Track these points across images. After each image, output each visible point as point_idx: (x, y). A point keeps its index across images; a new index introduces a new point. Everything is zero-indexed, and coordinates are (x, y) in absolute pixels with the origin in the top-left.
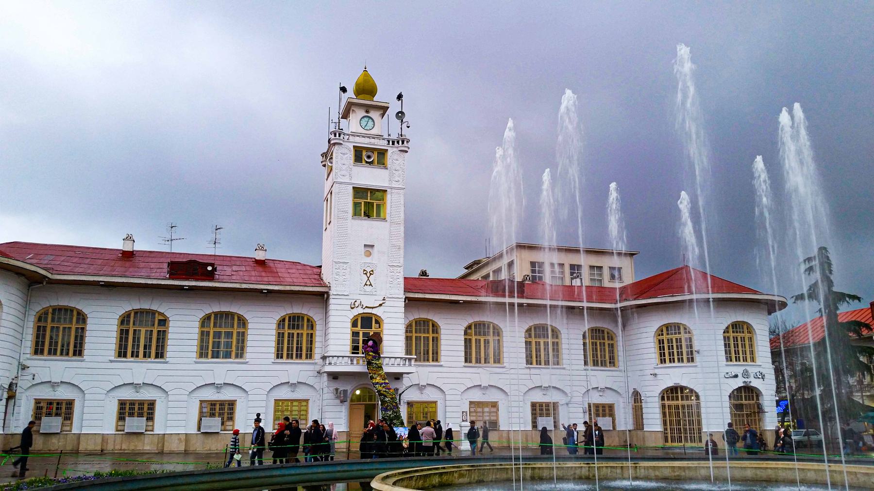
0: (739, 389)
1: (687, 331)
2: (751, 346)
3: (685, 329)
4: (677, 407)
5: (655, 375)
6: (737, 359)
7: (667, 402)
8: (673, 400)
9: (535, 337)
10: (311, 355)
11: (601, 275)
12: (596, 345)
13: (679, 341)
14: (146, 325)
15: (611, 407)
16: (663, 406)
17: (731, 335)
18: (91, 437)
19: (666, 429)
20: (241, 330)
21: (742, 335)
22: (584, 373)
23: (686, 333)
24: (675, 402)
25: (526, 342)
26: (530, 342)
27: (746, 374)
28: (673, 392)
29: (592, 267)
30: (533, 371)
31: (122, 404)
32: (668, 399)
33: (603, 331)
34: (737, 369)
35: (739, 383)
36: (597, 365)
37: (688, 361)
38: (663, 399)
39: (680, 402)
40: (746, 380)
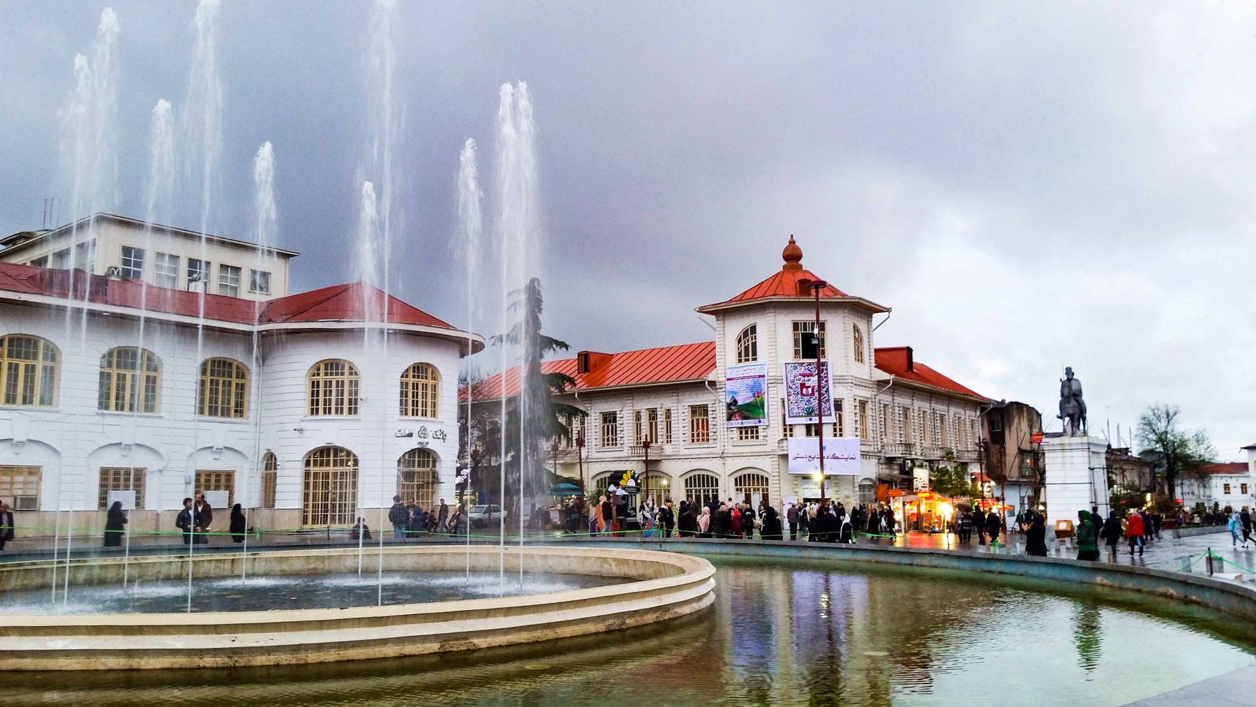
0: (412, 453)
1: (352, 371)
2: (434, 396)
3: (351, 368)
4: (326, 475)
5: (301, 430)
6: (415, 413)
7: (312, 469)
8: (322, 465)
9: (118, 366)
10: (241, 412)
11: (237, 280)
12: (217, 385)
13: (340, 384)
14: (27, 357)
15: (229, 476)
16: (307, 475)
17: (411, 380)
18: (287, 514)
19: (306, 506)
20: (49, 364)
21: (424, 381)
22: (192, 425)
23: (237, 377)
24: (324, 469)
25: (102, 374)
26: (109, 375)
27: (423, 433)
28: (324, 454)
29: (224, 267)
30: (109, 420)
31: (105, 473)
32: (315, 465)
33: (230, 365)
34: (412, 424)
35: (413, 444)
36: (216, 414)
37: (350, 413)
38: (308, 463)
39: (331, 469)
40: (423, 440)
